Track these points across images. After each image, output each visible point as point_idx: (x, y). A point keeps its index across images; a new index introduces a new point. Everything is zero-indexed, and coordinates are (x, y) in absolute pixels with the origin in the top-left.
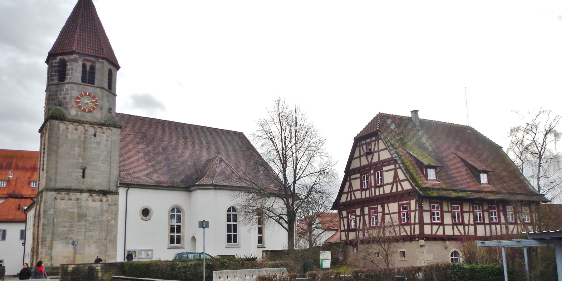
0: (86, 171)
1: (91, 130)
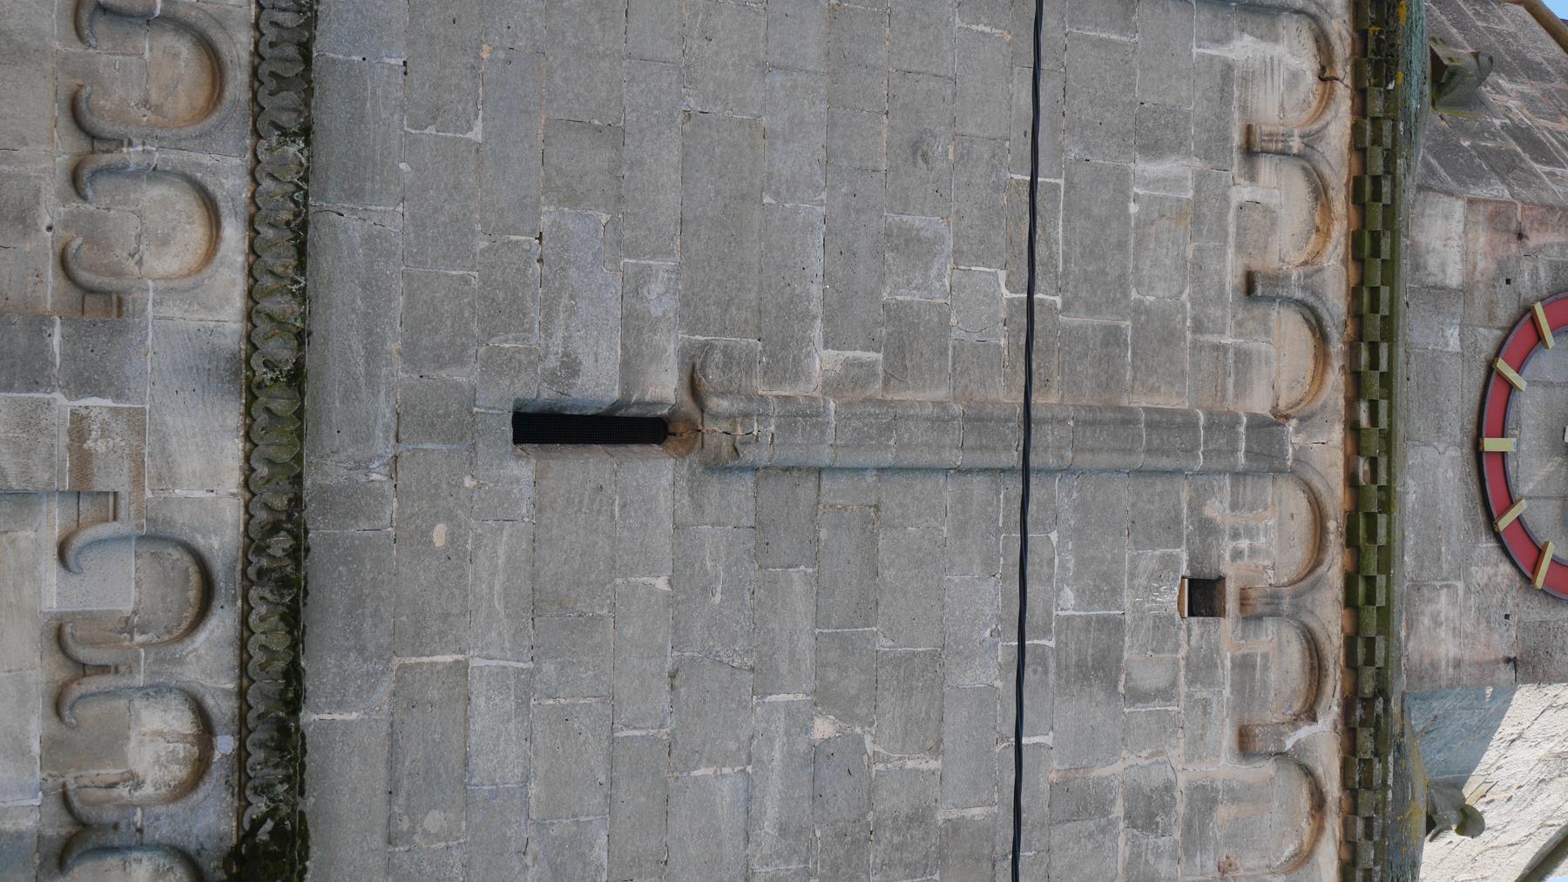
0: (654, 473)
1: (1268, 537)
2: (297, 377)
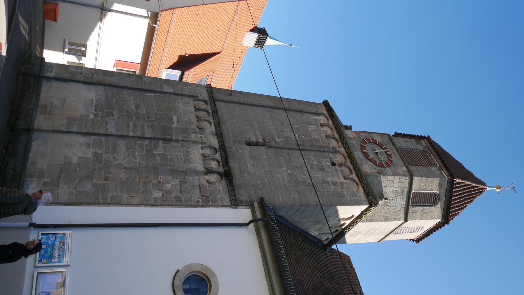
1: (339, 159)
2: (221, 134)
